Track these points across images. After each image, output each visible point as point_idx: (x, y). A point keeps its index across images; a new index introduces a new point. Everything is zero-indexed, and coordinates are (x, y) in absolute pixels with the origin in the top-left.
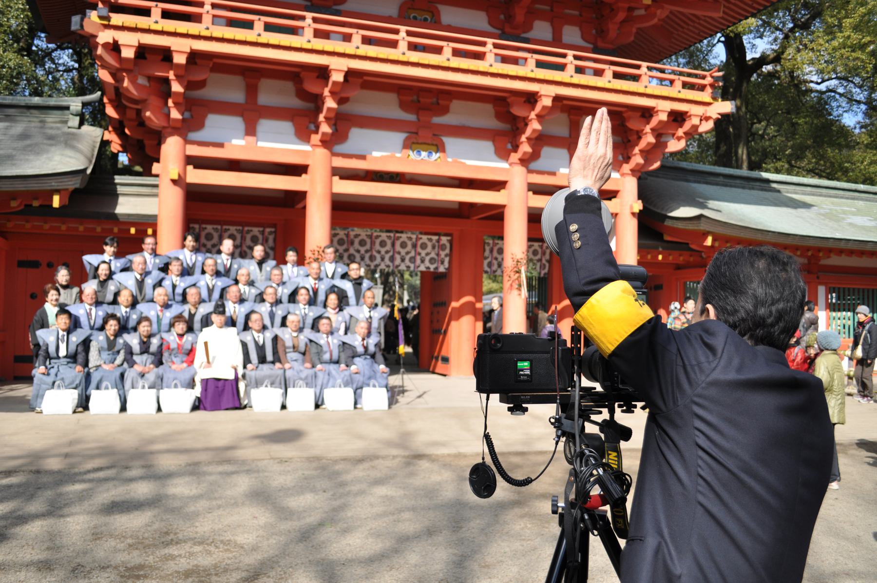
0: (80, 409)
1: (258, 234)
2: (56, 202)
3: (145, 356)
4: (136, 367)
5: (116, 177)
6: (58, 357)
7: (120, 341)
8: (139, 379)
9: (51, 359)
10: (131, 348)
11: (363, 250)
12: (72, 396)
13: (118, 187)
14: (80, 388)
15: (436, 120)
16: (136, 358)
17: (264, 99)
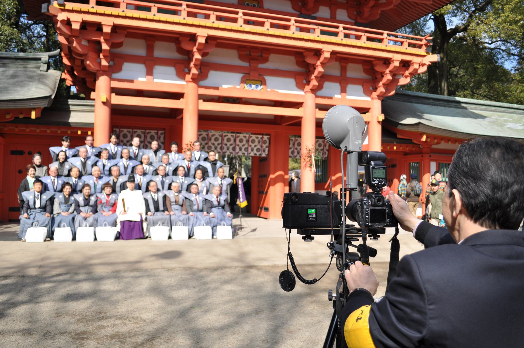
0: (48, 239)
1: (154, 134)
2: (33, 115)
3: (87, 207)
4: (81, 214)
5: (69, 100)
6: (35, 208)
8: (84, 221)
9: (31, 209)
11: (216, 143)
12: (44, 231)
14: (48, 227)
15: (261, 66)
16: (81, 208)
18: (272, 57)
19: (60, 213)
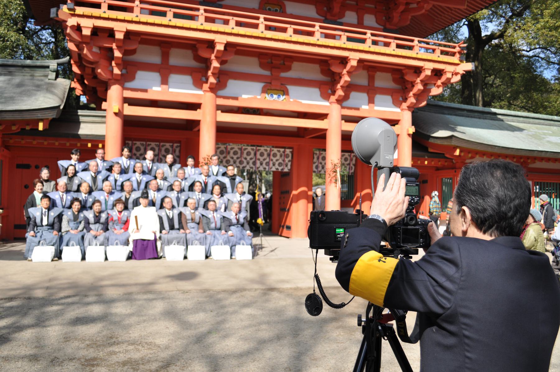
0: (56, 259)
1: (169, 147)
2: (41, 127)
4: (91, 232)
6: (42, 226)
7: (82, 215)
8: (94, 239)
9: (37, 226)
10: (88, 220)
11: (235, 157)
12: (51, 250)
13: (80, 117)
14: (56, 245)
15: (283, 75)
16: (91, 226)
17: (173, 61)
18: (295, 65)
19: (69, 231)
